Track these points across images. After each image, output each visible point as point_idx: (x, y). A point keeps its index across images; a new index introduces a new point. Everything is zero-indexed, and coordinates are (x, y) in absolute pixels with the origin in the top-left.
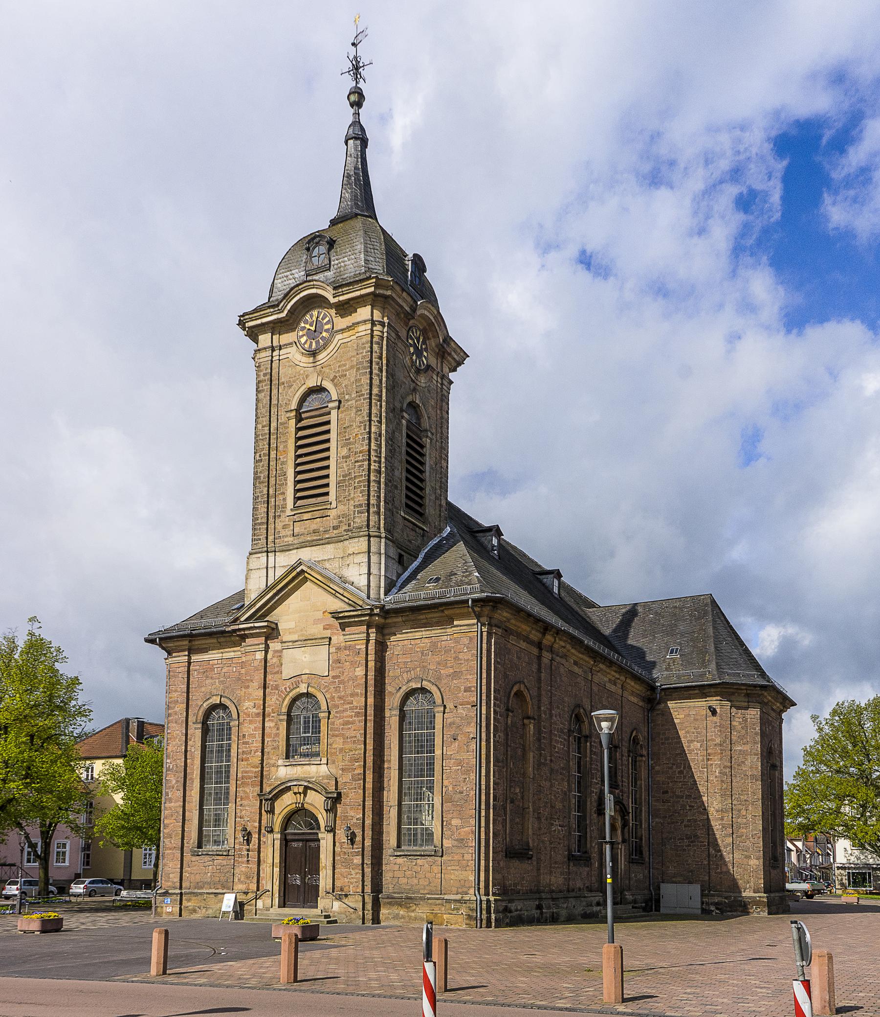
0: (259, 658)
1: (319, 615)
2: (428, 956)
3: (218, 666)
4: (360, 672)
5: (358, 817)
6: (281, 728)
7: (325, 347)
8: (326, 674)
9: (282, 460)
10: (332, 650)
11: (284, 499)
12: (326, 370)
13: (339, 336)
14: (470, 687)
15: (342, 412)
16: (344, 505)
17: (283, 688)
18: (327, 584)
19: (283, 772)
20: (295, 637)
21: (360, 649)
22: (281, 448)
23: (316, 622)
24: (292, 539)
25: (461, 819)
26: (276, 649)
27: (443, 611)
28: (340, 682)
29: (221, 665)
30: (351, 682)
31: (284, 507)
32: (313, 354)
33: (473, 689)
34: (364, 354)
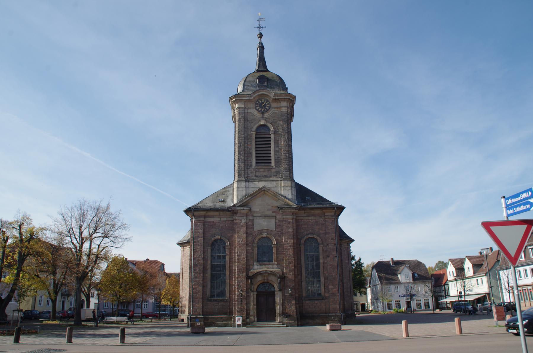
0: (244, 222)
1: (270, 207)
2: (493, 300)
3: (218, 223)
4: (290, 230)
5: (293, 285)
6: (254, 250)
7: (268, 110)
8: (275, 230)
9: (249, 148)
10: (277, 221)
11: (251, 162)
12: (268, 120)
13: (273, 110)
14: (333, 238)
15: (276, 135)
16: (278, 168)
17: (254, 234)
18: (276, 196)
19: (257, 268)
20: (259, 215)
21: (290, 222)
22: (249, 143)
23: (269, 210)
24: (255, 177)
25: (333, 286)
26: (250, 219)
27: (322, 210)
28: (280, 233)
29: (219, 223)
30: (287, 234)
31: (251, 165)
32: (263, 113)
33: (334, 239)
34: (285, 117)
